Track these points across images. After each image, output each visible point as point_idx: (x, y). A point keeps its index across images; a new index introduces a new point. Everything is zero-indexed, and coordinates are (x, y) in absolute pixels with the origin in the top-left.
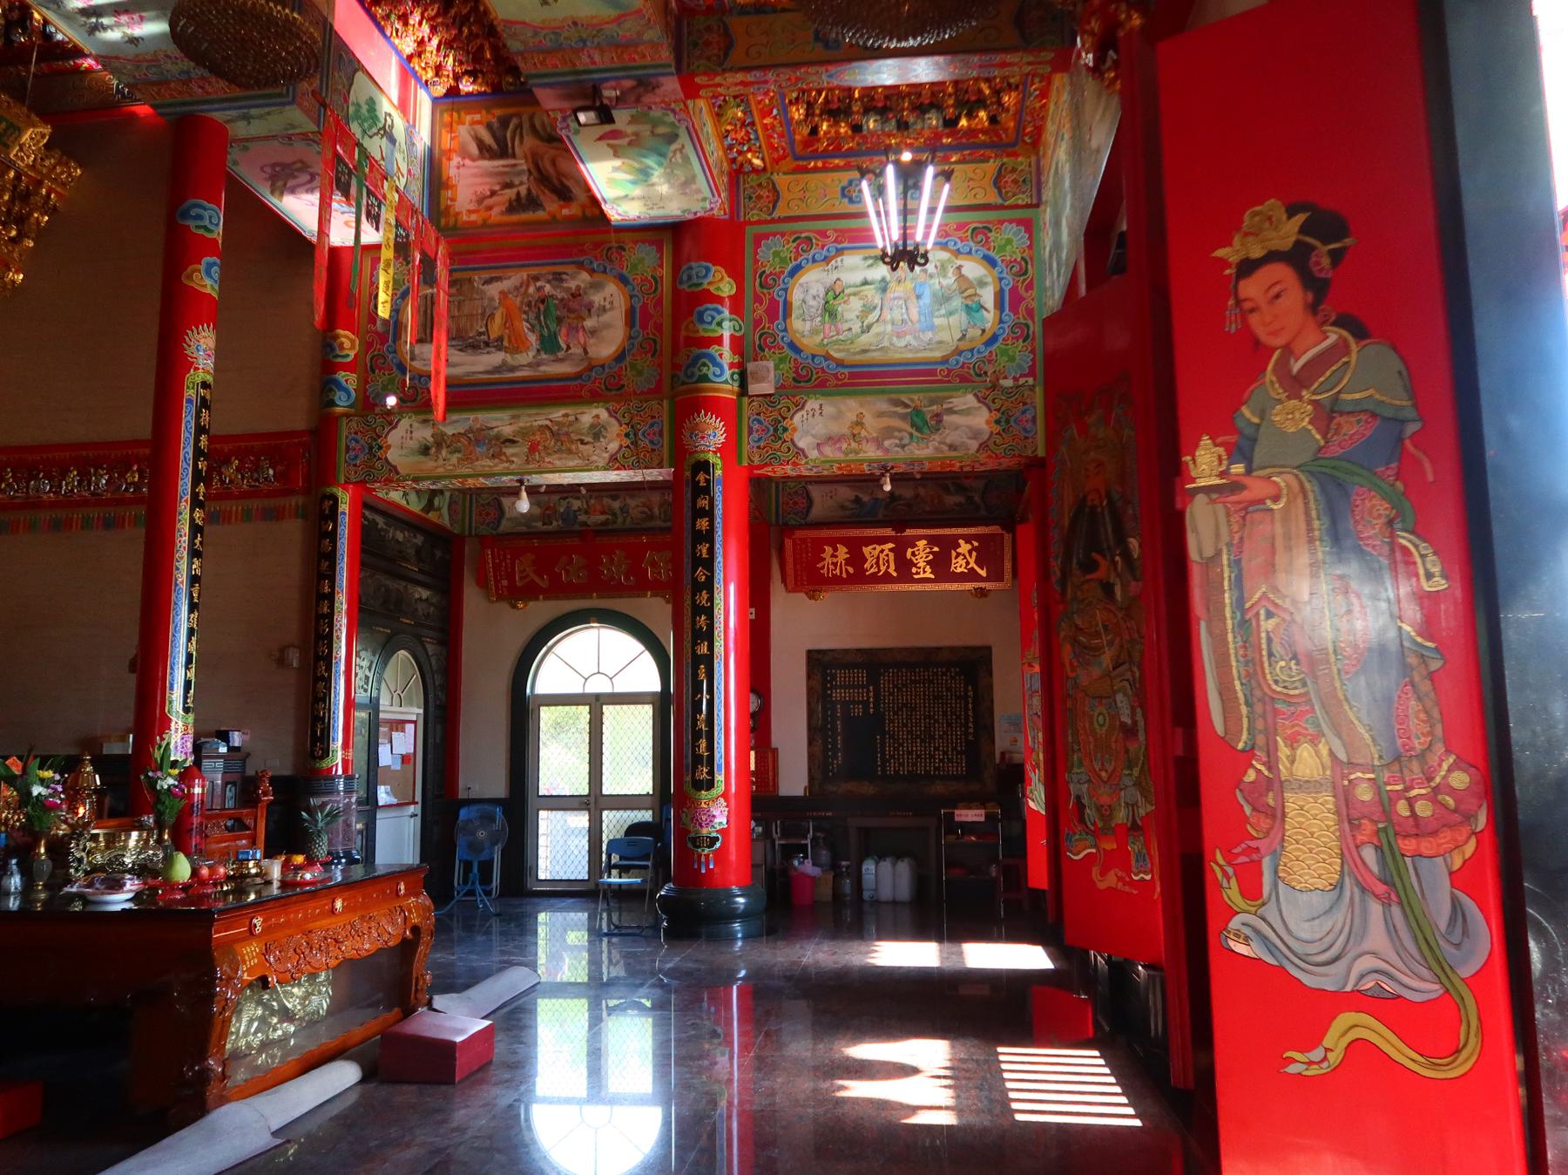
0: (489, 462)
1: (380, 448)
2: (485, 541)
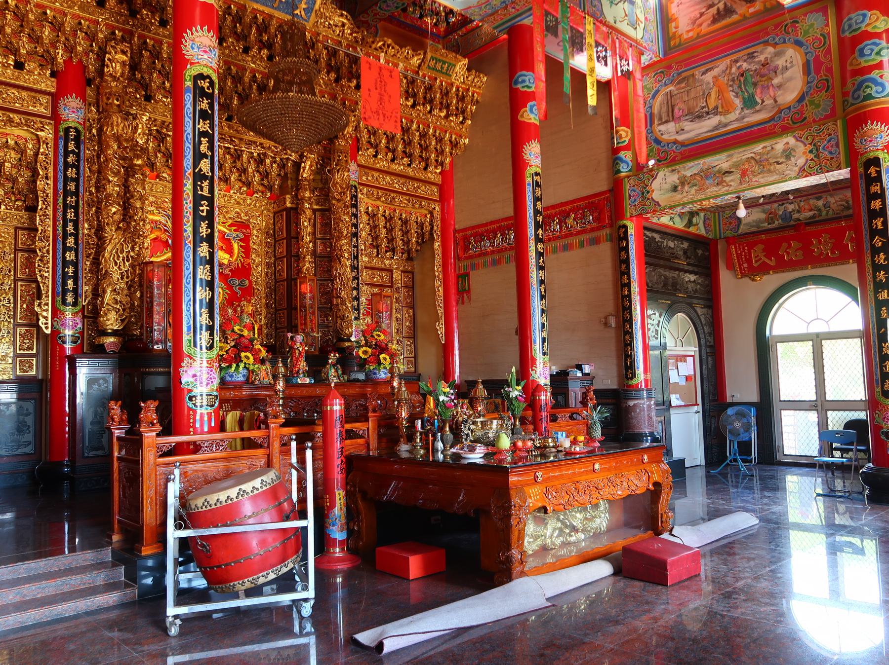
0: (715, 189)
1: (648, 192)
2: (729, 241)
